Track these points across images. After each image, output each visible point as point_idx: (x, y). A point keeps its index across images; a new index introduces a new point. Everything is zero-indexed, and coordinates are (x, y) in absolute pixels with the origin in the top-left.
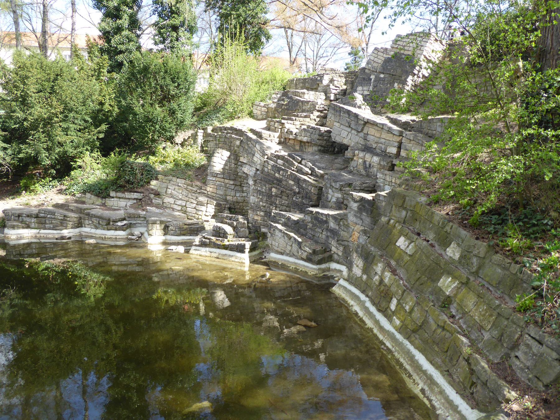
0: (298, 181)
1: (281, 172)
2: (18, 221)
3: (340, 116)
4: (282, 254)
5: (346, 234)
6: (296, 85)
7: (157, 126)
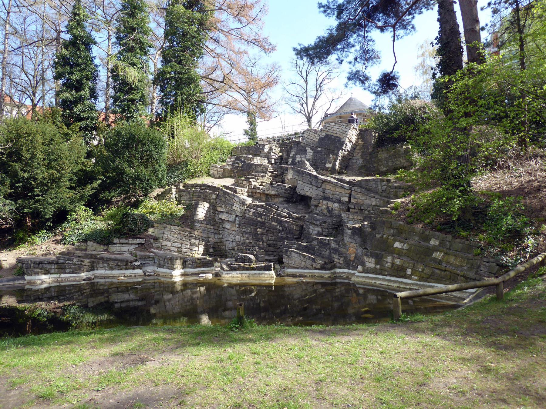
0: (280, 222)
1: (263, 217)
2: (38, 268)
3: (303, 177)
4: (297, 268)
5: (344, 250)
6: (241, 151)
7: (145, 184)
